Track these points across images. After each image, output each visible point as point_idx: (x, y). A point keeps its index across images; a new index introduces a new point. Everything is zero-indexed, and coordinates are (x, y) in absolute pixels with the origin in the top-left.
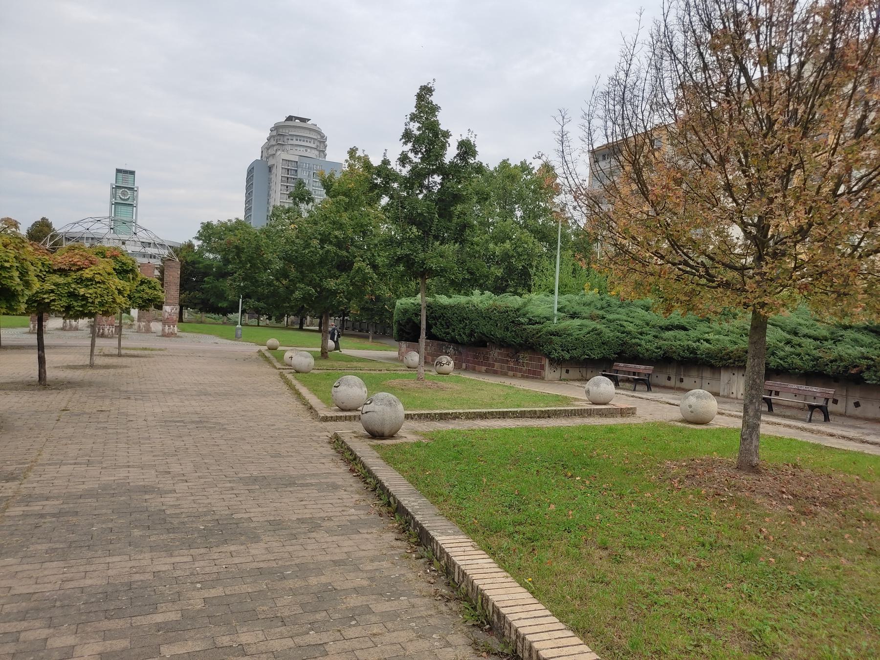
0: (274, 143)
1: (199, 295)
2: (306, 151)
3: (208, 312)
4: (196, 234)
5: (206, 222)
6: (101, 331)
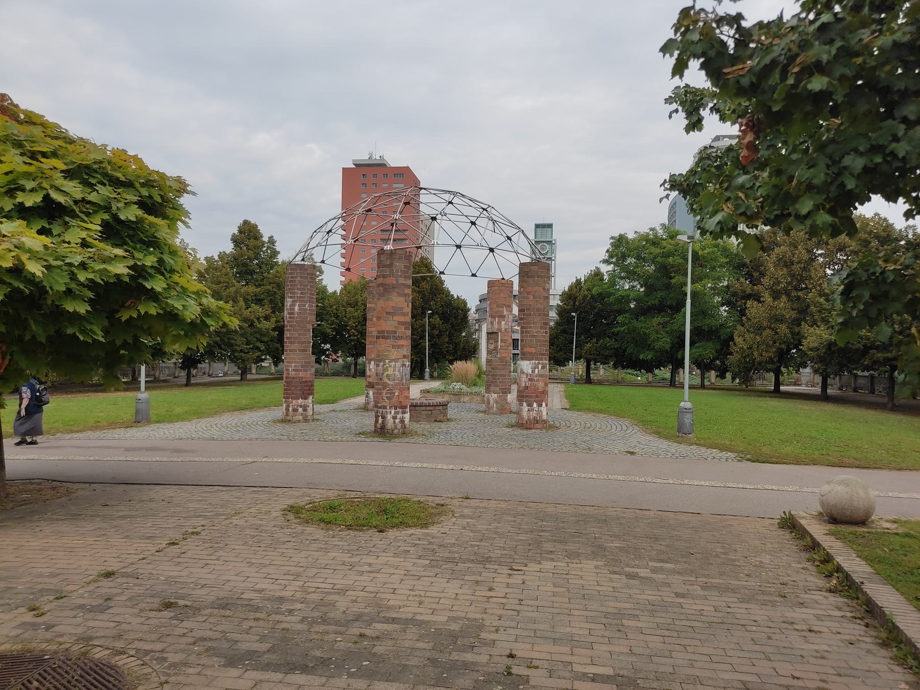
1: (610, 342)
3: (627, 367)
4: (604, 256)
5: (617, 235)
6: (380, 420)
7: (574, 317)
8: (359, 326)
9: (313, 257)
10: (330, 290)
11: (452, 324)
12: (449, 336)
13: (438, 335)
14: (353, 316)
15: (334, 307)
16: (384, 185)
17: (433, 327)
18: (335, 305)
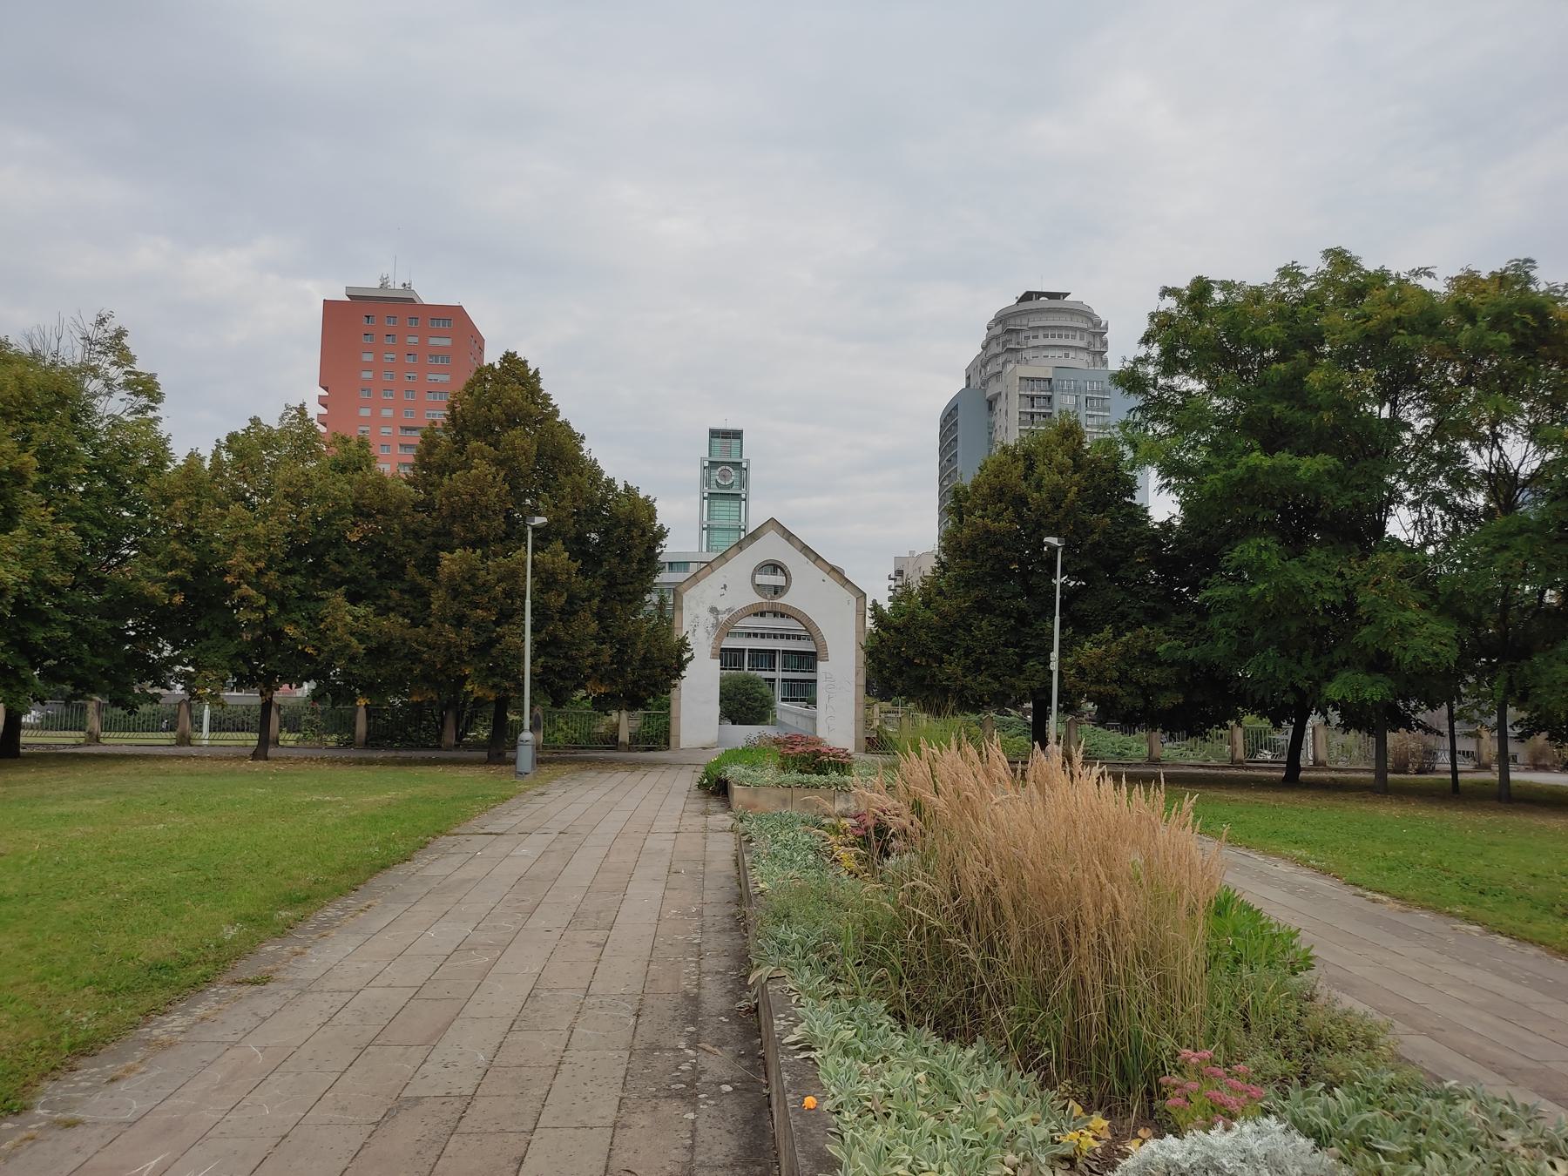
0: (999, 350)
2: (1067, 356)
7: (1054, 549)
8: (272, 575)
9: (125, 341)
10: (179, 452)
11: (610, 576)
12: (599, 616)
13: (562, 611)
14: (247, 536)
15: (180, 503)
16: (411, 339)
17: (546, 581)
18: (182, 495)
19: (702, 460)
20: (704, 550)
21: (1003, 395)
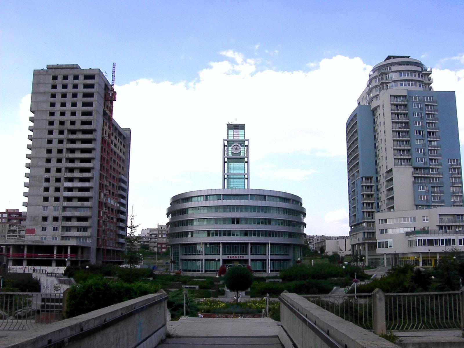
19: (224, 140)
20: (226, 187)
21: (381, 107)
